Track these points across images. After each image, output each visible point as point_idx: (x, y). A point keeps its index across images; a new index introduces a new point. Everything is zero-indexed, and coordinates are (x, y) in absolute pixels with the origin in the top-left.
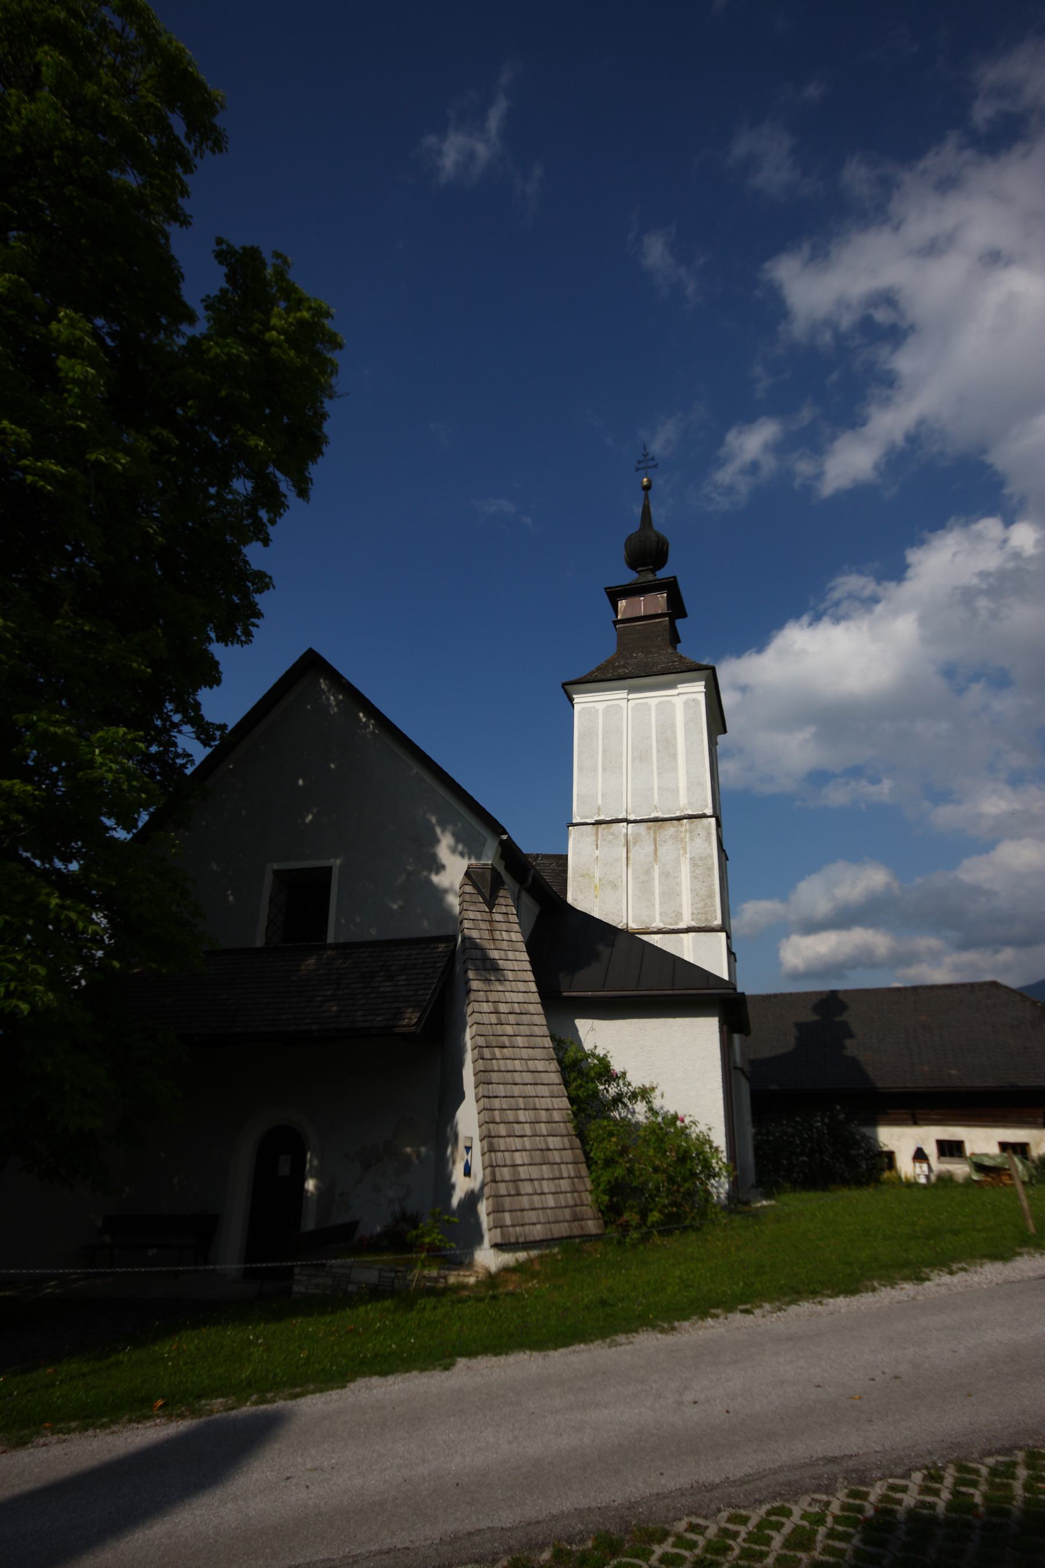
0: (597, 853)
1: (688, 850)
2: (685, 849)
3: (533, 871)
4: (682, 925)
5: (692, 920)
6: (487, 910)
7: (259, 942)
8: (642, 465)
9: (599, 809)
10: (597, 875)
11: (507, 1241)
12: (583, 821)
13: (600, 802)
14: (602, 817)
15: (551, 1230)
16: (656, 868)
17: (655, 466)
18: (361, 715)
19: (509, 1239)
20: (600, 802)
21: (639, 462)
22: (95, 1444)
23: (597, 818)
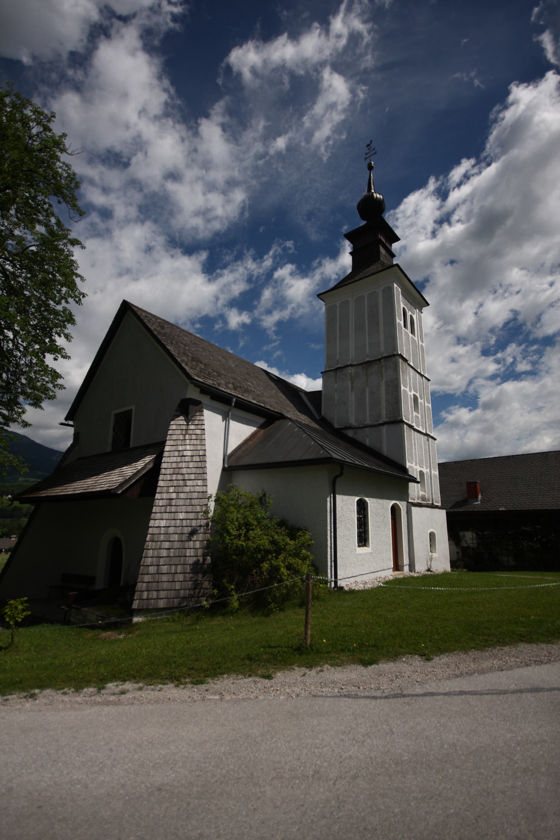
0: (336, 386)
1: (384, 377)
2: (382, 376)
3: (234, 399)
4: (381, 421)
5: (386, 418)
6: (185, 423)
7: (108, 451)
8: (368, 155)
9: (338, 361)
10: (336, 398)
11: (141, 608)
12: (330, 369)
13: (338, 358)
14: (339, 366)
15: (173, 602)
16: (367, 389)
17: (375, 153)
18: (313, 346)
19: (143, 607)
20: (338, 358)
21: (366, 154)
22: (103, 652)
23: (336, 367)
